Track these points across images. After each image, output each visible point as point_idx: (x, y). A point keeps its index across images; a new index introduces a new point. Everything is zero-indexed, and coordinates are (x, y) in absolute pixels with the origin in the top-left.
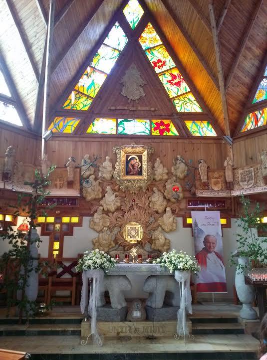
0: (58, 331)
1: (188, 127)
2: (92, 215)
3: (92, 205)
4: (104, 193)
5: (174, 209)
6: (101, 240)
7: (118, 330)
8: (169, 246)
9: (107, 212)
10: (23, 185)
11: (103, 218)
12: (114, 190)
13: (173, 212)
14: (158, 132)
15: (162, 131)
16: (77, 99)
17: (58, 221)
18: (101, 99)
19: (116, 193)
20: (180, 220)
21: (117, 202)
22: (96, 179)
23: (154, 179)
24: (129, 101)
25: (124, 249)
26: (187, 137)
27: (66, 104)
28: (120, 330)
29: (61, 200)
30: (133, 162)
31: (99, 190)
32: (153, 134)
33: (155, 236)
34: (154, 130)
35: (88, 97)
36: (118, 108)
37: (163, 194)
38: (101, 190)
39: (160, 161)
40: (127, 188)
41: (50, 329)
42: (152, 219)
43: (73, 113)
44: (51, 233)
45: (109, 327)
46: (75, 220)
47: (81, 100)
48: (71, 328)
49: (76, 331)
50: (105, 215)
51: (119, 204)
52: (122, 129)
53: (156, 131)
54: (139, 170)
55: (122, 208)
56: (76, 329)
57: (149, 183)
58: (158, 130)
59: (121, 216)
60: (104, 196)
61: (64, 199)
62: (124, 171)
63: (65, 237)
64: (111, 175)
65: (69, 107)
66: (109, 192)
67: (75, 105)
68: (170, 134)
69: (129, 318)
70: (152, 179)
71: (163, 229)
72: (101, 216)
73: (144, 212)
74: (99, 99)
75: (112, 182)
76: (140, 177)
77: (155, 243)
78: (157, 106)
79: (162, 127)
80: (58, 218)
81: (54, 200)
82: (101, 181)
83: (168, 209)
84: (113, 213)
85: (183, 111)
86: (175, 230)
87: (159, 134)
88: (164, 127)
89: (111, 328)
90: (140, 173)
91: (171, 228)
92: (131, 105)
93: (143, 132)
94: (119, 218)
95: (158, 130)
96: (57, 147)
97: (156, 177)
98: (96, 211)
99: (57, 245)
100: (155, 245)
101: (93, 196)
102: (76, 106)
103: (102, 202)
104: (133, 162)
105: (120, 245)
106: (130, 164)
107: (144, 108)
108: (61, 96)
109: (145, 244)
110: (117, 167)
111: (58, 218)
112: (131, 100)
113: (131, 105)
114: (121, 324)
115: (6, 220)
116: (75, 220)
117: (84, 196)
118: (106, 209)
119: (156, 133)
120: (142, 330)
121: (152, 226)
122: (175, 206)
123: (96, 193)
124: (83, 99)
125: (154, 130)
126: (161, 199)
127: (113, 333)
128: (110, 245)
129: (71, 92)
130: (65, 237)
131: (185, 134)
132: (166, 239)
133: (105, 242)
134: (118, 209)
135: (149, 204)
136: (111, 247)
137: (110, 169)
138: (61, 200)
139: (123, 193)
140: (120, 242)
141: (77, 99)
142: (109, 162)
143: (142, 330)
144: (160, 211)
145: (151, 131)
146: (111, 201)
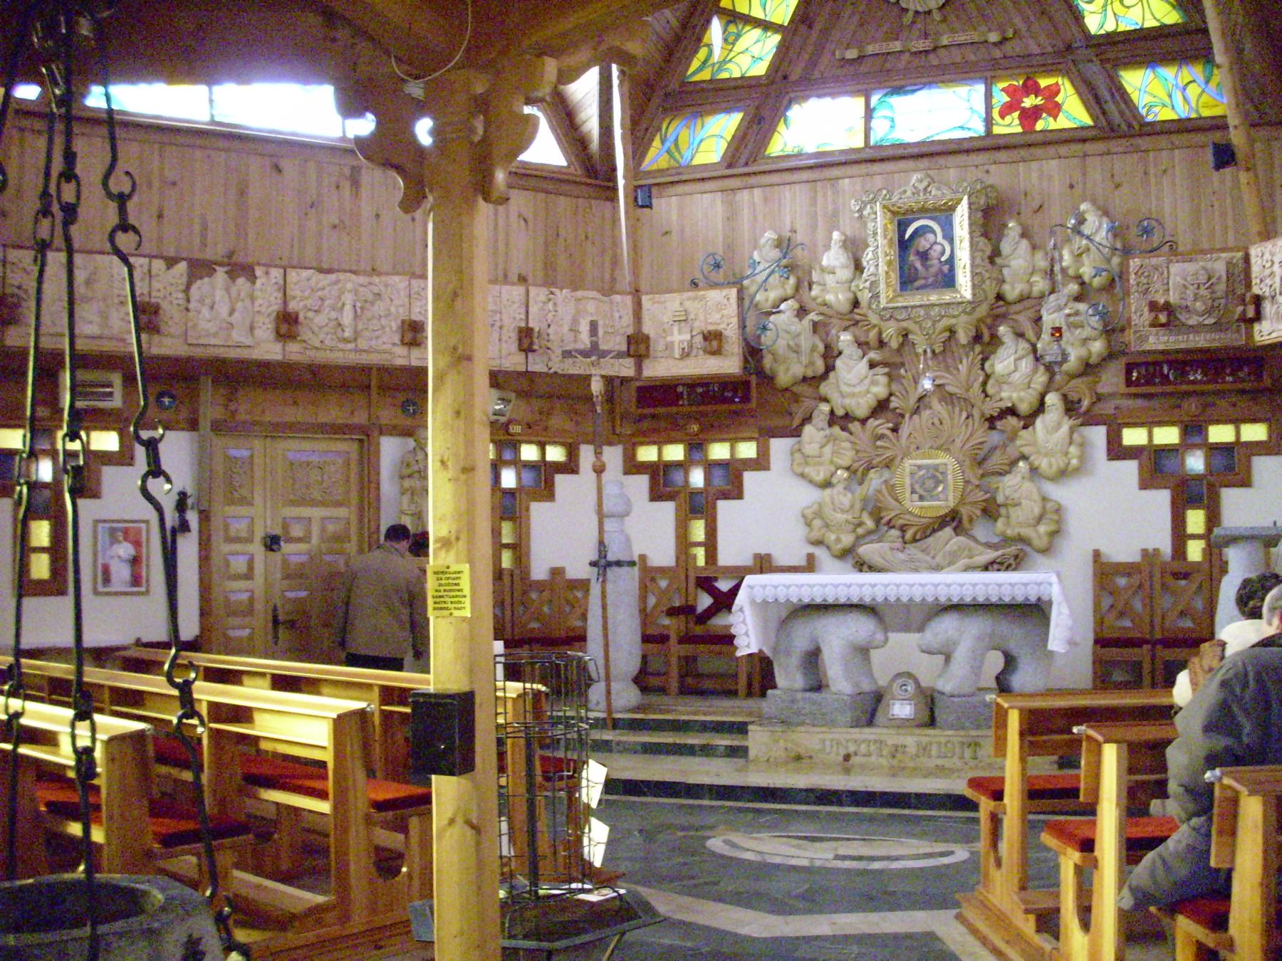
0: (692, 746)
1: (1129, 90)
2: (796, 433)
3: (796, 398)
4: (830, 355)
5: (1073, 396)
6: (828, 511)
7: (847, 748)
8: (1058, 522)
9: (841, 420)
10: (438, 458)
11: (830, 439)
12: (862, 345)
13: (1071, 407)
14: (1017, 122)
15: (1030, 116)
16: (729, 41)
17: (697, 456)
18: (810, 27)
19: (873, 355)
20: (1098, 435)
21: (873, 383)
22: (802, 312)
23: (999, 297)
24: (908, 18)
25: (903, 537)
26: (1124, 127)
27: (695, 64)
28: (852, 748)
29: (700, 390)
30: (923, 244)
31: (813, 349)
32: (997, 130)
33: (1007, 493)
34: (1002, 116)
35: (766, 26)
36: (870, 49)
37: (1034, 347)
38: (821, 347)
39: (1019, 230)
40: (906, 335)
41: (670, 740)
42: (995, 437)
43: (722, 94)
44: (678, 493)
45: (824, 741)
46: (747, 450)
47: (740, 45)
48: (723, 741)
49: (739, 747)
50: (836, 429)
51: (880, 391)
52: (888, 123)
53: (1008, 119)
54: (946, 268)
55: (892, 405)
56: (736, 743)
57: (983, 310)
58: (1016, 114)
59: (888, 433)
60: (830, 368)
61: (707, 384)
62: (895, 278)
63: (721, 505)
64: (851, 296)
65: (705, 75)
66: (846, 352)
67: (724, 62)
68: (1062, 122)
69: (880, 718)
70: (992, 296)
71: (1034, 470)
72: (828, 431)
73: (964, 415)
74: (803, 28)
75: (858, 317)
76: (947, 297)
77: (1008, 517)
78: (1010, 20)
79: (1029, 102)
80: (1193, 430)
81: (680, 389)
82: (817, 318)
83: (1052, 399)
84: (863, 421)
85: (1110, 27)
86: (1077, 470)
87: (1019, 130)
88: (1039, 101)
89: (828, 743)
90: (948, 281)
91: (1062, 465)
92: (915, 33)
93: (962, 128)
94: (882, 437)
95: (1016, 114)
96: (674, 217)
97: (1006, 288)
98: (807, 419)
99: (698, 530)
100: (1008, 524)
101: (797, 370)
102: (728, 66)
103: (824, 389)
104: (923, 244)
105: (890, 525)
106: (912, 250)
107: (962, 38)
108: (678, 39)
109: (971, 520)
110: (869, 269)
111: (1193, 430)
112: (917, 12)
113: (915, 33)
114: (857, 733)
115: (549, 458)
116: (747, 450)
117: (768, 372)
118: (840, 412)
119: (1010, 126)
120: (912, 750)
121: (996, 460)
122: (1080, 388)
123: (805, 360)
124: (752, 35)
125: (1002, 116)
126: (1026, 365)
127: (833, 755)
128: (860, 524)
129: (708, 22)
130: (721, 505)
131: (1117, 118)
132: (1044, 499)
133: (841, 517)
134: (881, 407)
135: (984, 383)
136: (860, 531)
137: (845, 273)
138: (700, 390)
139: (891, 358)
140: (887, 516)
141: (729, 41)
142: (841, 251)
143: (912, 750)
144: (1024, 408)
145: (989, 121)
146: (855, 382)
